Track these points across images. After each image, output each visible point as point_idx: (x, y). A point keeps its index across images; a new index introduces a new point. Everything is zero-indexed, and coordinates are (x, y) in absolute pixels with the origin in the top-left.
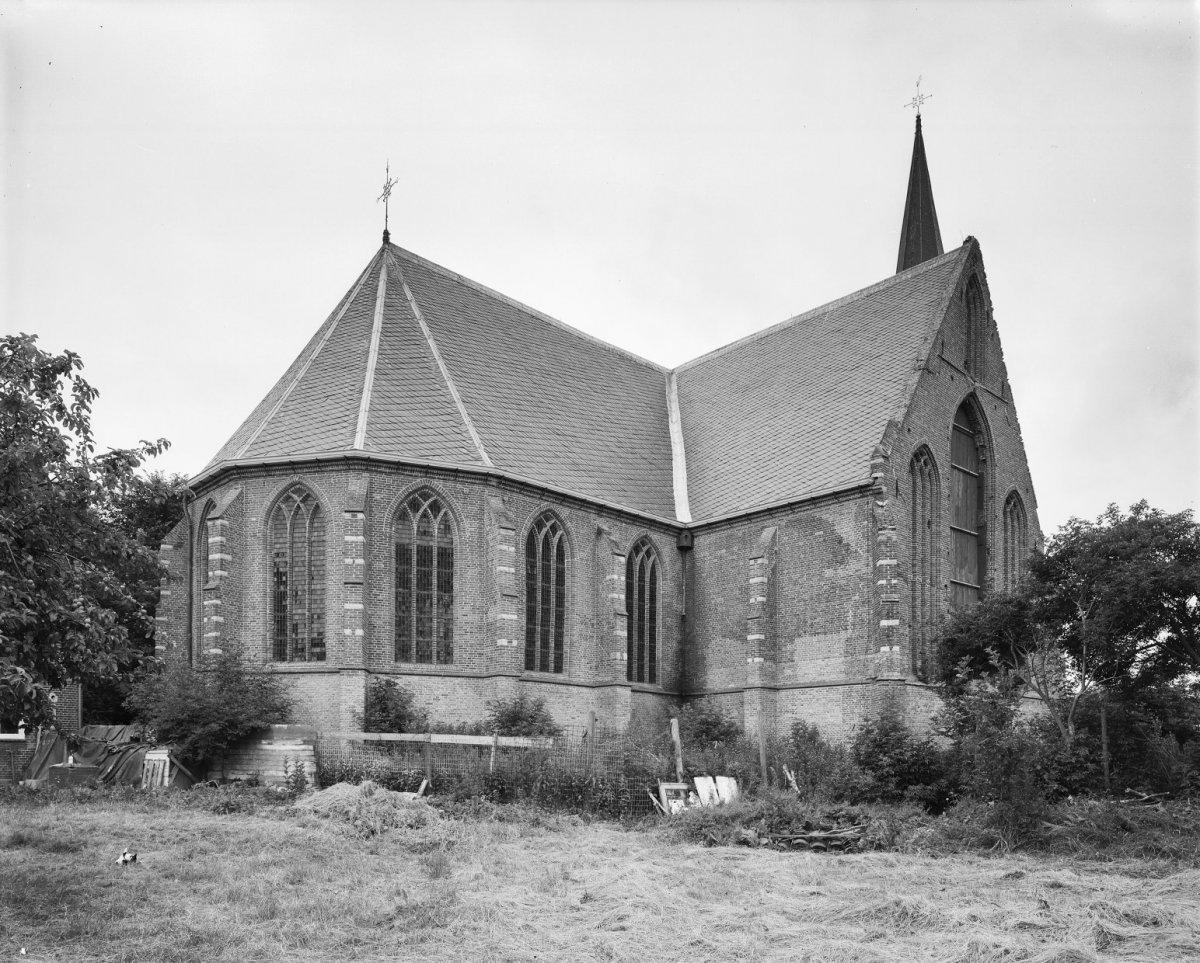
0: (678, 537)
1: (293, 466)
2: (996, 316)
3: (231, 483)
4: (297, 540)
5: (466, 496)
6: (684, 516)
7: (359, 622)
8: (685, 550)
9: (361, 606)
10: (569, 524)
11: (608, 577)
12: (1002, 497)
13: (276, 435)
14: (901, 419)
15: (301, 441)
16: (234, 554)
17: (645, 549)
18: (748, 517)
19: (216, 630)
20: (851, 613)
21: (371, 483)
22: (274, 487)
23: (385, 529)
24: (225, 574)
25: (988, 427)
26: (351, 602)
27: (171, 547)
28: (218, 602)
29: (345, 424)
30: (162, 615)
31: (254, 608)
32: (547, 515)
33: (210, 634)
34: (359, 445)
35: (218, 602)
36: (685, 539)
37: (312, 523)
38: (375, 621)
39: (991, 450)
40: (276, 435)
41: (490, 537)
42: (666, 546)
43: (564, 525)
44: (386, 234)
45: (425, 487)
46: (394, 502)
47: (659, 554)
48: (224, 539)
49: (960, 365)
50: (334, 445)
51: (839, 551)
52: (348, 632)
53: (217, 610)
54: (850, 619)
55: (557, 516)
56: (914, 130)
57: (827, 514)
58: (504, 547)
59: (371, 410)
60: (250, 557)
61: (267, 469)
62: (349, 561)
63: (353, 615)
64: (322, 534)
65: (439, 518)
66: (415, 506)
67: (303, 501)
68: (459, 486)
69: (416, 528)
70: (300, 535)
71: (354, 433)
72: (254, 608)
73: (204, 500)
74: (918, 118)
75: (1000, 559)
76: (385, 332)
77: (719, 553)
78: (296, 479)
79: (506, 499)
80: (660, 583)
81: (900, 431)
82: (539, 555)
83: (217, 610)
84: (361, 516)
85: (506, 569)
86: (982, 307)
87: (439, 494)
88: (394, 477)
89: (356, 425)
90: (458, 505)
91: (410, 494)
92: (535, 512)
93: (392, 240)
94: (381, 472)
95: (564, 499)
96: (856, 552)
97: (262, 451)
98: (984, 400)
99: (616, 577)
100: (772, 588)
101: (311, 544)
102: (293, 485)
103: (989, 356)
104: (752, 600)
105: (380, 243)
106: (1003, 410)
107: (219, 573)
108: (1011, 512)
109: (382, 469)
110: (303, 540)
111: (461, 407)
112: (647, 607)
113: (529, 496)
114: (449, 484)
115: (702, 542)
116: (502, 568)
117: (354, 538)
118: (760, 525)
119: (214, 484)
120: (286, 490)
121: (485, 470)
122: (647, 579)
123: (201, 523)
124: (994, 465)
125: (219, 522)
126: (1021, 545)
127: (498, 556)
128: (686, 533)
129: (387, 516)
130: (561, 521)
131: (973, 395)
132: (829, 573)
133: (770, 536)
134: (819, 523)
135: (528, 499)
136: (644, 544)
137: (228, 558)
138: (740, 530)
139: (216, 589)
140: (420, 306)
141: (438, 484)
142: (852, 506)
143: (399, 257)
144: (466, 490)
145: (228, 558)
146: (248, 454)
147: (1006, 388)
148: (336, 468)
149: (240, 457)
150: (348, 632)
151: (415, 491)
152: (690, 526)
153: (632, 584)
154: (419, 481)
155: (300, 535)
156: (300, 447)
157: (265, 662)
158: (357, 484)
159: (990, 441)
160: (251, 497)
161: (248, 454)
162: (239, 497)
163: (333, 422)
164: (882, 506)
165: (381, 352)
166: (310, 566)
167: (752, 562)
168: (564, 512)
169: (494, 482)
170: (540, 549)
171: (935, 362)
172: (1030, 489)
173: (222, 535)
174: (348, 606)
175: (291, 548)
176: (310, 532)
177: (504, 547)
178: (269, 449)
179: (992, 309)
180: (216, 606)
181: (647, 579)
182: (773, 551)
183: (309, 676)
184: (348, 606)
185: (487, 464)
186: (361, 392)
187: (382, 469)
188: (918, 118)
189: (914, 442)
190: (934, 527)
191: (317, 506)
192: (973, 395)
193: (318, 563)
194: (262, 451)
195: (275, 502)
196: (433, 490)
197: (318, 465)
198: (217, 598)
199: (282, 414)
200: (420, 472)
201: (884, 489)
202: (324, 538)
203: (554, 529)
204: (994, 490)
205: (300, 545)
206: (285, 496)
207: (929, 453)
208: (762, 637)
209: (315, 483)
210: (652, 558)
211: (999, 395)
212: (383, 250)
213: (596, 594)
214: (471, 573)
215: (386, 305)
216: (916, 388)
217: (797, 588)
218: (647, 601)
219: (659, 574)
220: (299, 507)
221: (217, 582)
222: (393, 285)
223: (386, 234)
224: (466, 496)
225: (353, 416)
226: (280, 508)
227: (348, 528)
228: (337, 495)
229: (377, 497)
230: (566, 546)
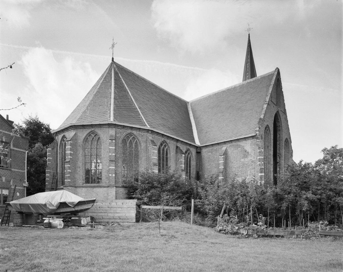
0: (196, 149)
1: (92, 126)
2: (283, 90)
3: (72, 130)
4: (93, 148)
5: (142, 136)
6: (198, 143)
7: (114, 172)
8: (199, 153)
9: (114, 168)
10: (169, 145)
11: (180, 160)
12: (284, 140)
13: (85, 117)
14: (263, 118)
15: (93, 118)
16: (74, 152)
17: (188, 152)
18: (218, 144)
19: (69, 174)
20: (249, 171)
21: (116, 131)
22: (86, 132)
23: (120, 145)
24: (71, 157)
25: (281, 120)
26: (111, 166)
27: (51, 149)
28: (70, 166)
29: (107, 114)
30: (48, 169)
31: (80, 168)
32: (164, 142)
33: (67, 175)
34: (112, 120)
35: (70, 166)
36: (199, 150)
37: (97, 143)
38: (117, 172)
39: (282, 127)
40: (85, 117)
41: (149, 148)
42: (193, 151)
43: (168, 145)
44: (113, 58)
45: (131, 133)
46: (122, 137)
47: (192, 154)
48: (71, 147)
49: (275, 103)
50: (104, 120)
51: (246, 154)
52: (110, 175)
53: (69, 168)
54: (249, 173)
55: (166, 142)
56: (248, 38)
57: (242, 143)
58: (154, 151)
59: (114, 110)
60: (78, 153)
61: (83, 126)
62: (111, 154)
63: (112, 170)
64: (100, 146)
65: (129, 142)
66: (128, 138)
67: (95, 136)
68: (140, 133)
69: (128, 145)
70: (94, 146)
71: (110, 116)
72: (80, 168)
73: (62, 135)
74: (249, 35)
75: (283, 158)
76: (115, 87)
77: (209, 154)
78: (93, 129)
79: (153, 137)
80: (192, 162)
81: (263, 121)
82: (161, 153)
83: (69, 168)
84: (114, 141)
85: (154, 157)
86: (280, 88)
87: (135, 135)
88: (122, 130)
89: (110, 114)
90: (140, 139)
91: (127, 135)
92: (161, 141)
93: (114, 60)
94: (119, 128)
95: (168, 137)
96: (251, 154)
97: (82, 121)
98: (280, 113)
99: (182, 160)
100: (226, 164)
101: (97, 148)
102: (92, 131)
103: (281, 101)
104: (220, 167)
105: (111, 61)
106: (284, 116)
107: (69, 157)
108: (286, 144)
109: (119, 128)
110: (94, 148)
111: (139, 110)
112: (188, 169)
113: (159, 136)
114: (138, 132)
115: (204, 151)
116: (154, 157)
117: (112, 148)
118: (221, 146)
119: (66, 130)
120: (90, 133)
121: (148, 129)
122: (189, 161)
123: (60, 142)
124: (282, 131)
125: (70, 142)
126: (288, 153)
127: (152, 153)
128: (199, 148)
129: (120, 141)
130: (167, 144)
131: (278, 112)
132: (242, 160)
133: (225, 149)
134: (239, 146)
135: (159, 137)
136: (188, 151)
137: (72, 152)
138: (215, 148)
139: (69, 162)
140: (124, 80)
141: (135, 132)
142: (249, 142)
143: (116, 66)
144: (142, 134)
145: (72, 152)
146: (77, 122)
147: (285, 110)
148: (105, 127)
149: (74, 122)
150: (110, 175)
151: (128, 134)
152: (200, 146)
153: (166, 162)
154: (129, 131)
155: (94, 146)
156: (93, 120)
157: (83, 184)
158: (112, 132)
159: (281, 124)
160: (78, 134)
161: (77, 122)
162: (75, 134)
163: (103, 113)
164: (259, 142)
165: (115, 93)
166: (97, 155)
167: (220, 157)
168: (168, 141)
169: (150, 132)
170: (162, 152)
171: (270, 102)
172: (290, 138)
173: (70, 146)
174: (110, 167)
175: (91, 150)
176: (97, 145)
177: (154, 151)
178: (84, 120)
179: (282, 88)
180: (69, 167)
181: (189, 161)
182: (226, 154)
183: (97, 188)
184: (110, 167)
185: (148, 127)
186: (110, 104)
187: (119, 128)
188: (249, 35)
189: (266, 124)
190: (269, 148)
191: (99, 138)
192: (278, 112)
193: (99, 154)
194: (82, 121)
195: (86, 136)
196: (133, 134)
197: (100, 126)
198: (69, 164)
199: (87, 110)
200: (130, 129)
201: (259, 137)
202: (101, 147)
203: (165, 146)
204: (282, 138)
205: (94, 149)
206: (89, 135)
207: (269, 127)
208: (223, 178)
209: (98, 131)
210: (190, 155)
211: (284, 112)
212: (112, 63)
213: (176, 164)
214: (143, 158)
215: (115, 80)
216: (266, 109)
217: (233, 164)
218: (188, 167)
219: (191, 159)
220: (93, 138)
221: (69, 160)
222: (116, 74)
223: (113, 58)
224: (142, 136)
225: (109, 112)
226: (87, 138)
227: (110, 144)
228: (105, 135)
229: (118, 136)
230: (168, 151)
